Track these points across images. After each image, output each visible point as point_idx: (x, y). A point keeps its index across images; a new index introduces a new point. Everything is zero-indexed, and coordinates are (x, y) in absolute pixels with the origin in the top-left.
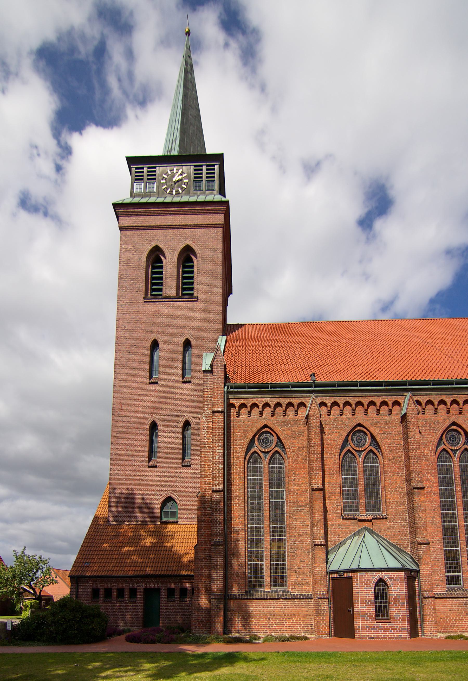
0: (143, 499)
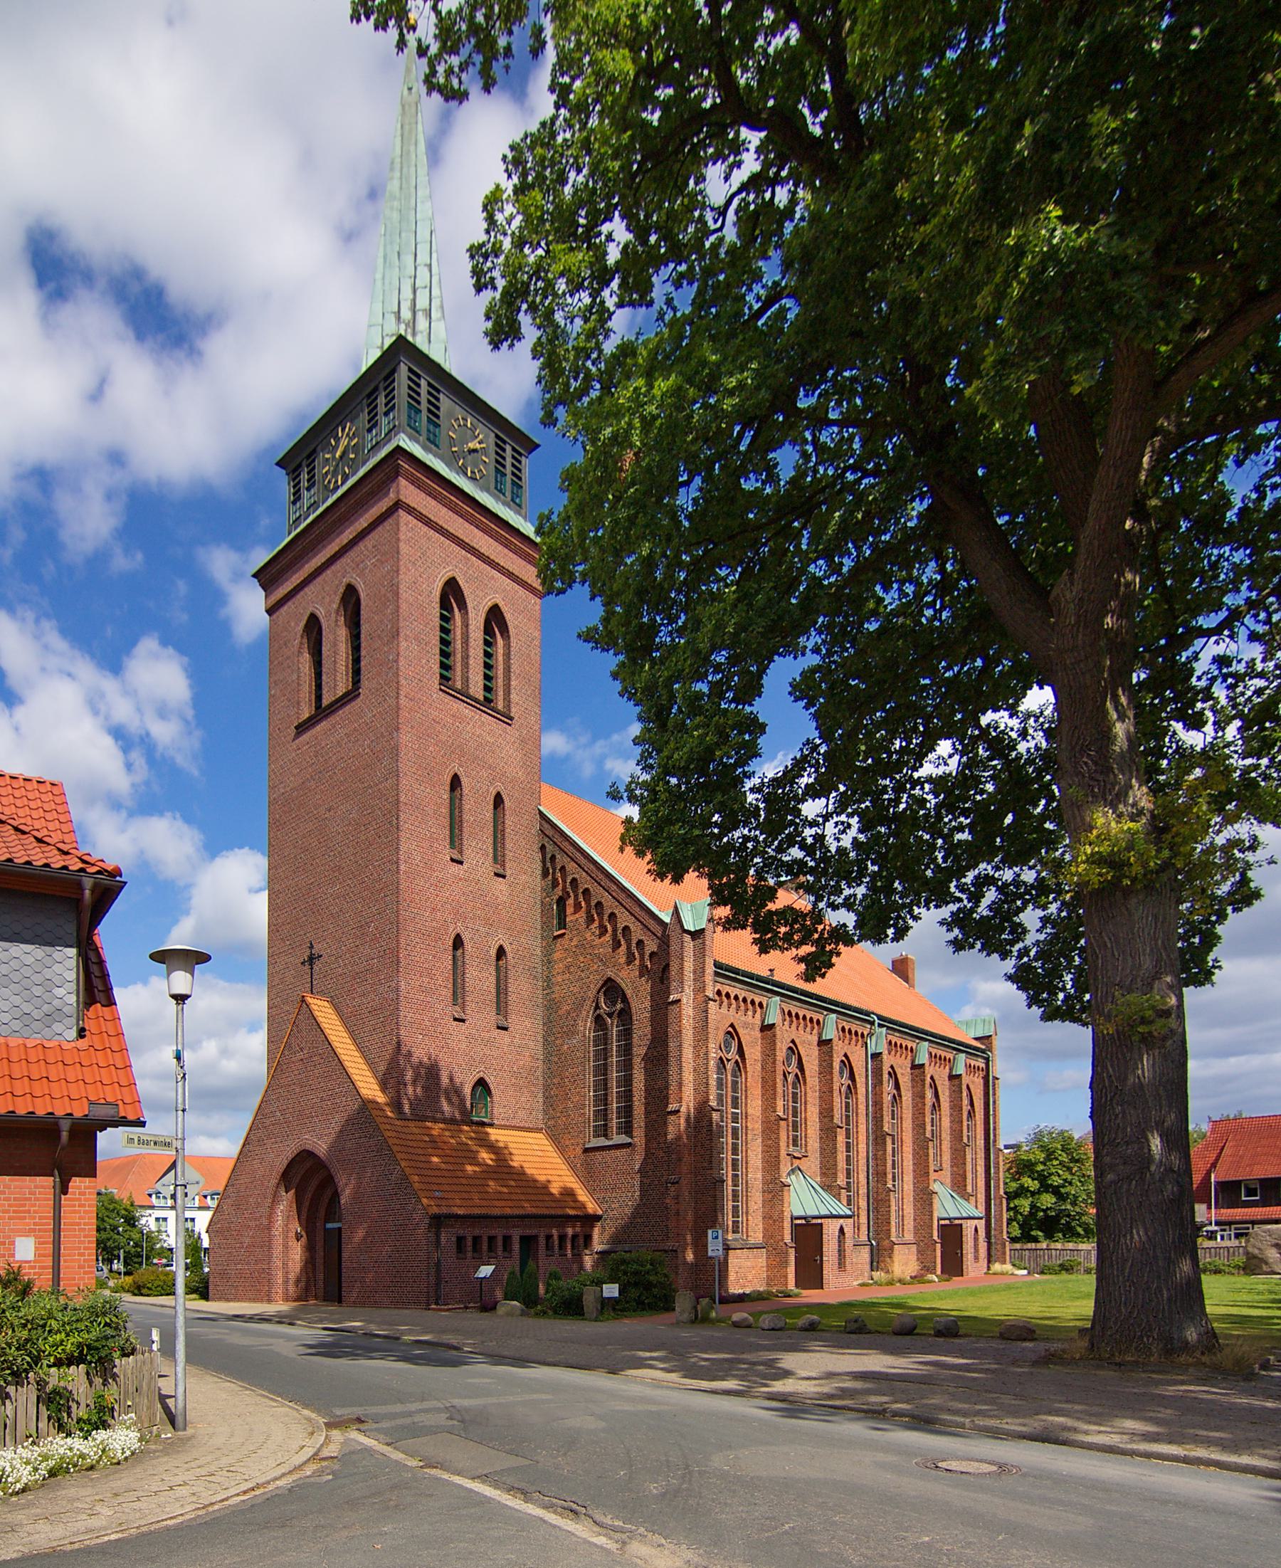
0: (451, 1079)
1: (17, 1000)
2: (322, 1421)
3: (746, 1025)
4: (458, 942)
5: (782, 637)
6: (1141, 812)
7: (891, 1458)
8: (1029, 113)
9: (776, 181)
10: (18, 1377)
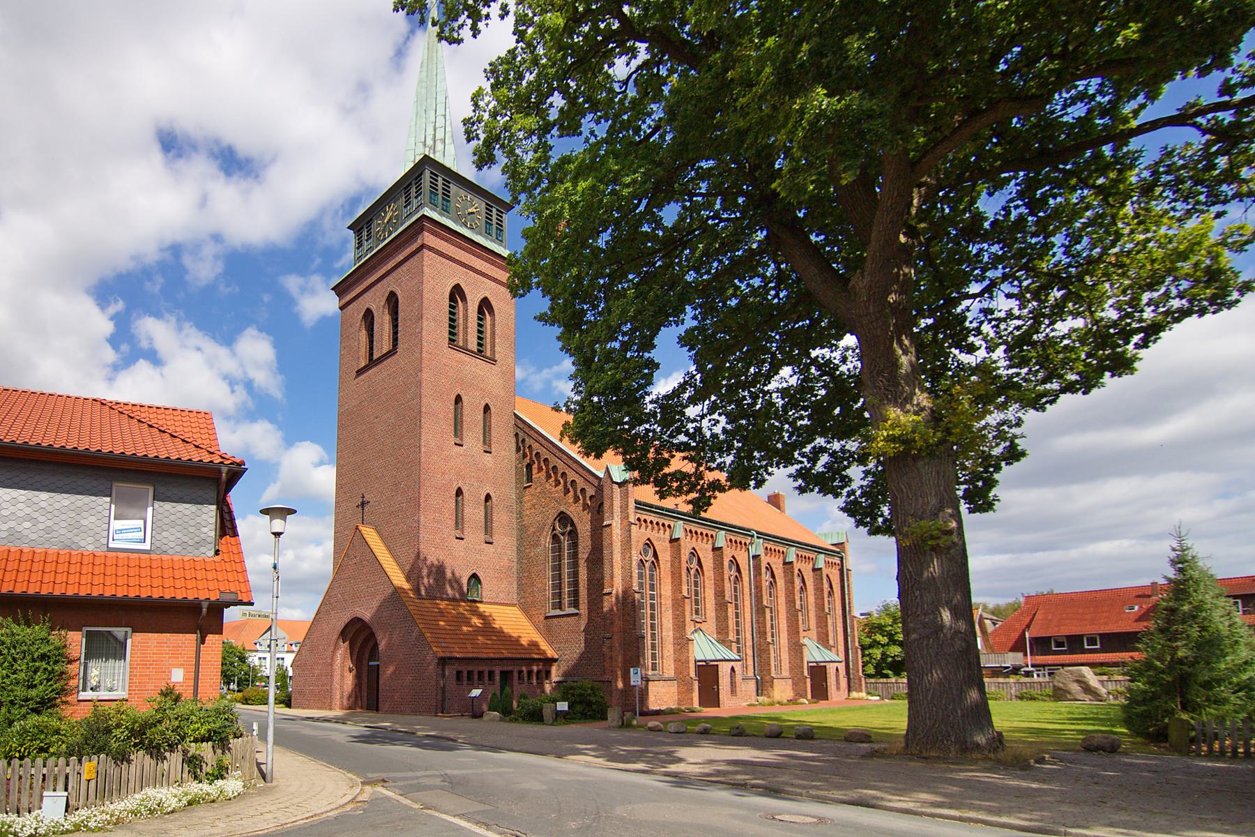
0: (453, 573)
1: (179, 535)
2: (359, 780)
3: (659, 539)
4: (459, 492)
5: (665, 313)
6: (923, 409)
7: (741, 812)
8: (805, 38)
9: (658, 64)
10: (172, 747)
